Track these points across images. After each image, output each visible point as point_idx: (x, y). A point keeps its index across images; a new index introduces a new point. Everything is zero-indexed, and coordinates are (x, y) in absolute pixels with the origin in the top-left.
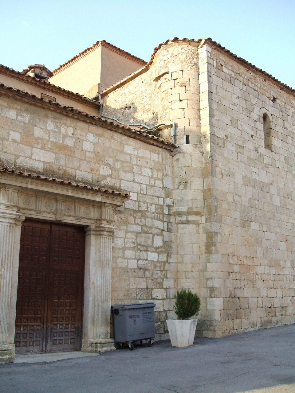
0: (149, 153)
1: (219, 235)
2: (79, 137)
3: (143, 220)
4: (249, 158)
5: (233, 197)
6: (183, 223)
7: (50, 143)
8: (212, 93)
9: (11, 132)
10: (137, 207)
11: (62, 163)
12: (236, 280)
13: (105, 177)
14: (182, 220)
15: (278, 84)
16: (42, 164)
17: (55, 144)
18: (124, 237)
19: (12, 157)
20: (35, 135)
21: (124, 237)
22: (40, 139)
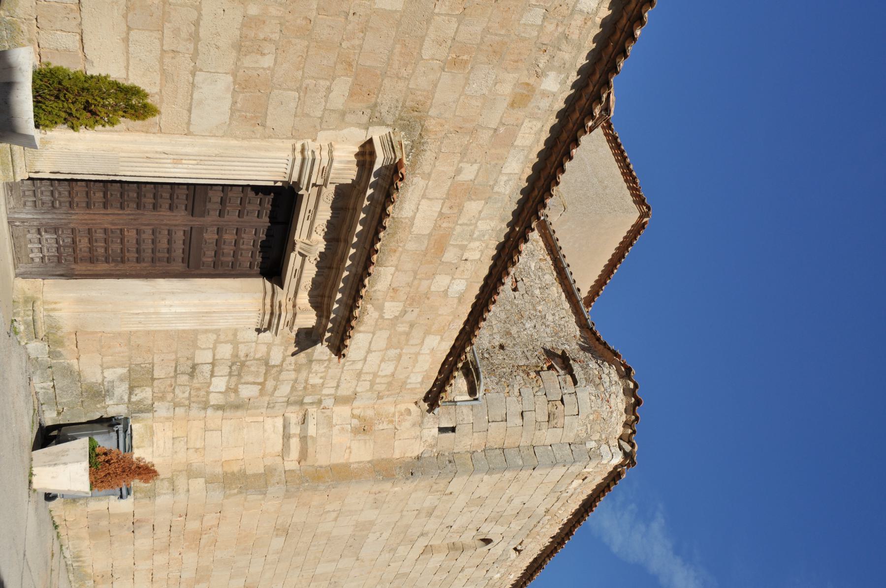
0: (424, 370)
1: (260, 497)
2: (461, 269)
3: (293, 367)
4: (408, 527)
5: (334, 511)
6: (284, 427)
7: (451, 225)
8: (534, 469)
9: (476, 167)
10: (319, 358)
11: (411, 246)
12: (171, 526)
13: (380, 309)
14: (291, 427)
15: (546, 555)
16: (410, 214)
17: (449, 234)
18: (258, 342)
19: (426, 168)
20: (468, 202)
21: (258, 342)
22: (460, 211)
